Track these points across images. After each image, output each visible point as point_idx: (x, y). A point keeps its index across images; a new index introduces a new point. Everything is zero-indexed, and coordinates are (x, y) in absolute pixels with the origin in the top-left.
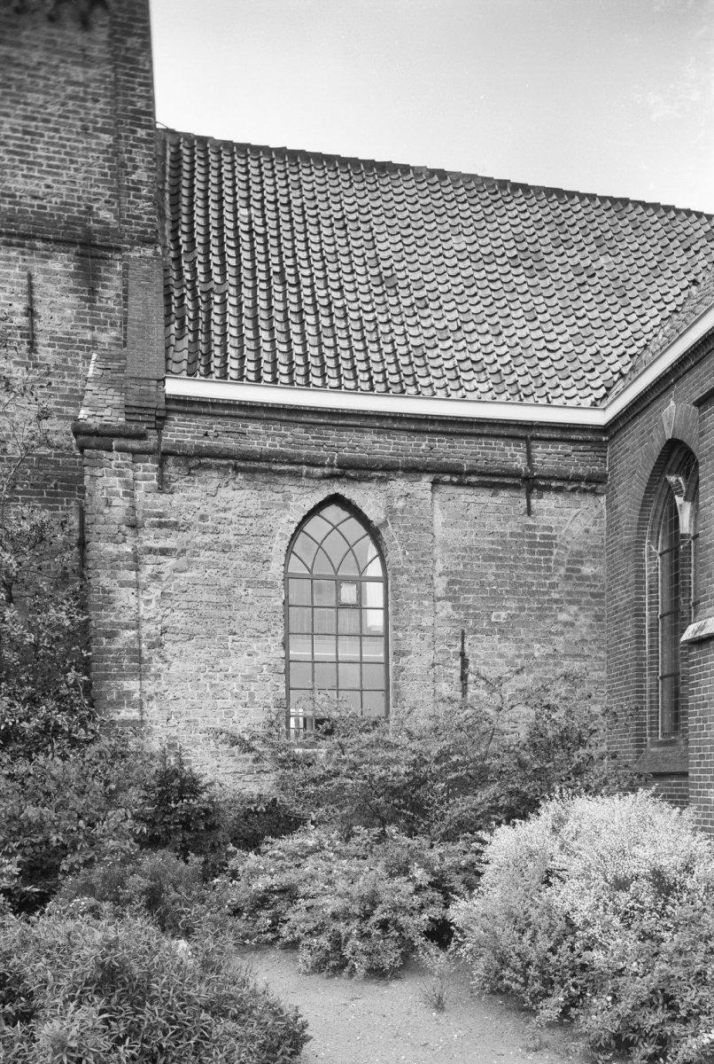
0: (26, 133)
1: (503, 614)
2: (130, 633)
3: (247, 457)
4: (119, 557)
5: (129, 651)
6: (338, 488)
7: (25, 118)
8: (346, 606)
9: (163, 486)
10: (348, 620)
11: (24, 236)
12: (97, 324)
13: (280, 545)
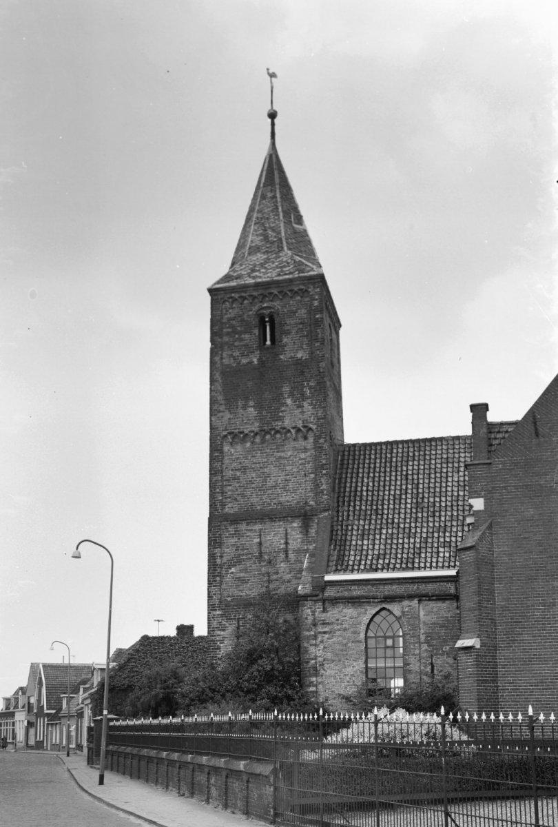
0: (286, 480)
1: (448, 647)
2: (313, 662)
3: (352, 598)
4: (310, 636)
5: (313, 668)
6: (384, 605)
7: (285, 476)
8: (388, 647)
9: (325, 610)
10: (389, 652)
11: (284, 517)
12: (309, 543)
13: (364, 627)
